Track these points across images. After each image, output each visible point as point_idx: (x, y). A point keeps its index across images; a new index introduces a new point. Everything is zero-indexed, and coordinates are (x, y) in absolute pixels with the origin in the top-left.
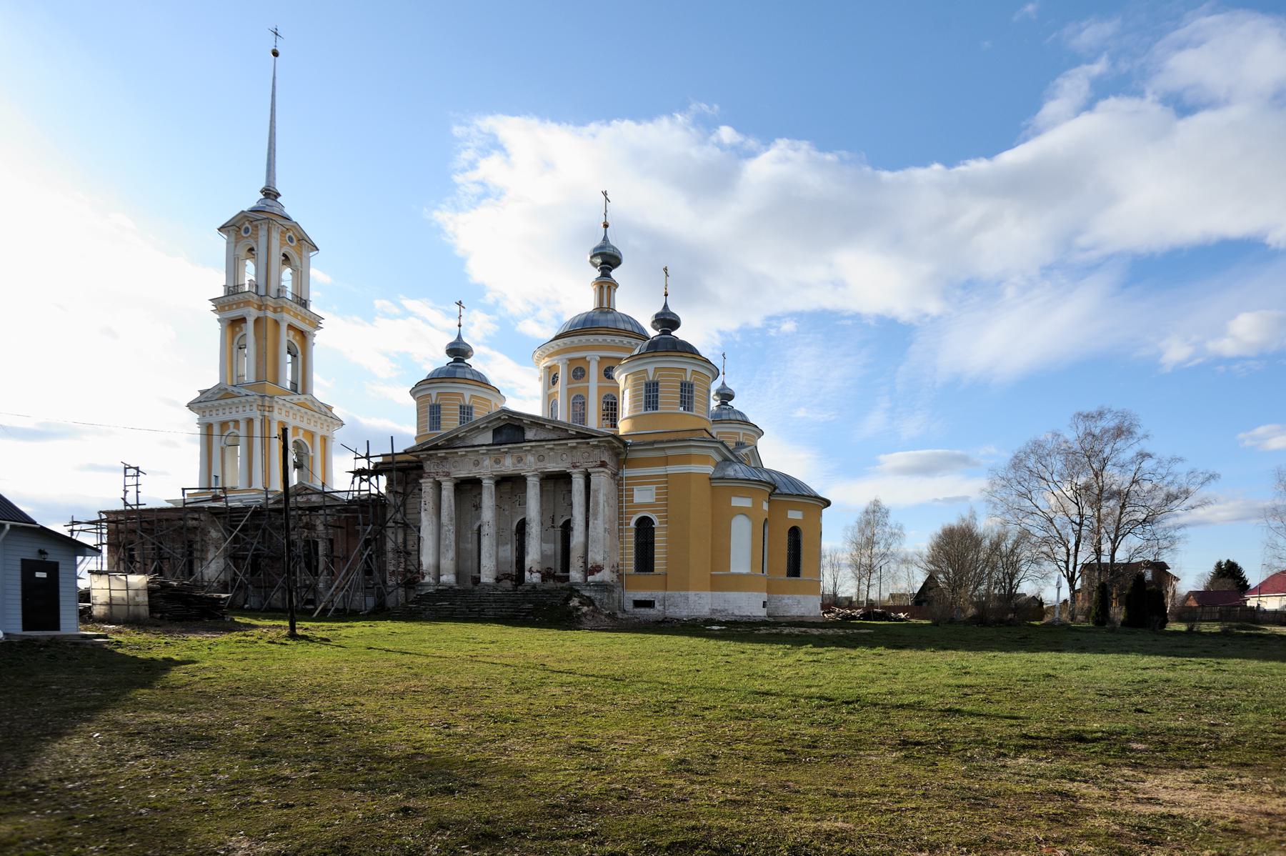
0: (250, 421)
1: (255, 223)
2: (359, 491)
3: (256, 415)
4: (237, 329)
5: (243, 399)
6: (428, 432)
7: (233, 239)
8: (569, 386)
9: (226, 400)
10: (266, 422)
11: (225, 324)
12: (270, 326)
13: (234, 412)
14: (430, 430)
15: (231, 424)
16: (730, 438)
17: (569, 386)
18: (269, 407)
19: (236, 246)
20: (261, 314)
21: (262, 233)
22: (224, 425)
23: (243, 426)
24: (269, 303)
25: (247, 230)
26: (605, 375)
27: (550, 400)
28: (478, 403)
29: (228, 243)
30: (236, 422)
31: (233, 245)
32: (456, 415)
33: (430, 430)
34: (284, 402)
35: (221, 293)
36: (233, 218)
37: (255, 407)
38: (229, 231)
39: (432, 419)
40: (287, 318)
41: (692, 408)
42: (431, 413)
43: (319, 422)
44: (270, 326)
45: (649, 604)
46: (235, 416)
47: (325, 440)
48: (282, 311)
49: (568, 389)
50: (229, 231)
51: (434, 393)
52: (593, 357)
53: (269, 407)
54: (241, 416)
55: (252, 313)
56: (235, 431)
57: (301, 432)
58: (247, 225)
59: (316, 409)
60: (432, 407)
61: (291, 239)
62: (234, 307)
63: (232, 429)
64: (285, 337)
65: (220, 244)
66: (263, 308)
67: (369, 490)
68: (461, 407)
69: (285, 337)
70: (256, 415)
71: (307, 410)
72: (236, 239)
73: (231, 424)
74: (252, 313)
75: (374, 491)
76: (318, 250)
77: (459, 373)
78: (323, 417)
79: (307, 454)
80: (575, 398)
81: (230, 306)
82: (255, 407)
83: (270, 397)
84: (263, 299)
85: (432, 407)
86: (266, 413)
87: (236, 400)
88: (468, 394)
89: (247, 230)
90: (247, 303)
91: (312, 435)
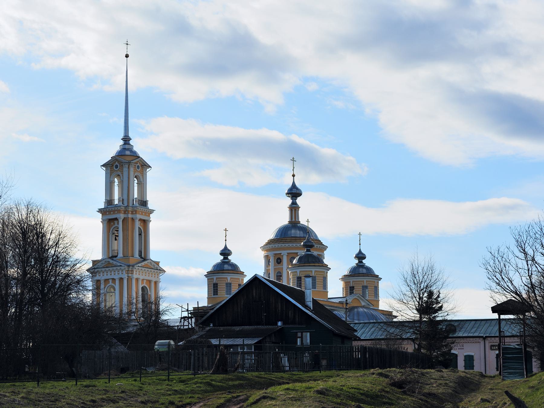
0: (121, 279)
1: (122, 164)
2: (184, 326)
3: (125, 276)
4: (112, 224)
5: (118, 268)
6: (213, 296)
7: (109, 171)
8: (275, 267)
9: (113, 268)
10: (129, 280)
11: (106, 222)
12: (130, 221)
13: (120, 274)
14: (213, 295)
15: (111, 281)
16: (372, 284)
17: (275, 267)
18: (131, 271)
19: (111, 175)
20: (126, 216)
21: (125, 169)
22: (106, 281)
23: (117, 282)
24: (129, 210)
25: (117, 167)
26: (280, 263)
27: (267, 272)
28: (234, 281)
29: (106, 173)
30: (114, 280)
31: (109, 174)
32: (224, 288)
33: (213, 295)
34: (139, 267)
35: (102, 206)
36: (109, 161)
37: (124, 271)
38: (107, 167)
39: (214, 292)
40: (139, 216)
41: (297, 279)
42: (214, 288)
43: (151, 273)
44: (130, 221)
45: (113, 263)
46: (113, 276)
47: (137, 280)
48: (136, 213)
49: (274, 268)
50: (107, 167)
51: (215, 278)
52: (284, 253)
53: (131, 271)
54: (117, 277)
55: (121, 216)
56: (113, 284)
57: (145, 281)
58: (117, 163)
59: (152, 267)
60: (214, 284)
61: (138, 167)
62: (112, 213)
63: (111, 283)
64: (138, 224)
65: (102, 173)
66: (127, 212)
67: (188, 326)
68: (226, 283)
69: (138, 224)
70: (125, 276)
71: (151, 270)
72: (111, 171)
73: (111, 281)
74: (121, 216)
75: (190, 327)
76: (151, 167)
77: (226, 267)
78: (156, 271)
79: (147, 294)
80: (277, 273)
81: (110, 212)
82: (124, 271)
83: (132, 266)
84: (127, 208)
85: (214, 284)
86: (130, 275)
87: (115, 268)
88: (229, 277)
89: (117, 167)
90: (119, 211)
91: (149, 281)
